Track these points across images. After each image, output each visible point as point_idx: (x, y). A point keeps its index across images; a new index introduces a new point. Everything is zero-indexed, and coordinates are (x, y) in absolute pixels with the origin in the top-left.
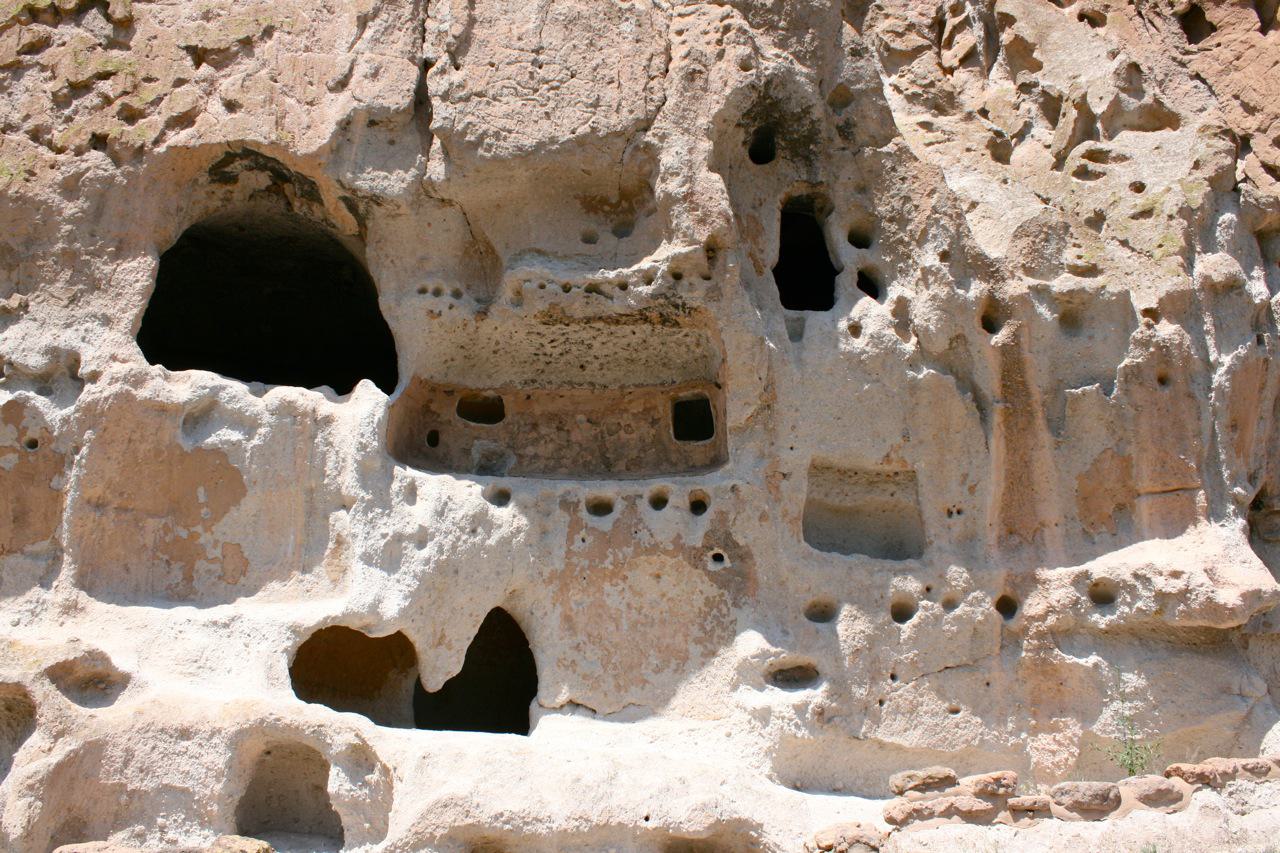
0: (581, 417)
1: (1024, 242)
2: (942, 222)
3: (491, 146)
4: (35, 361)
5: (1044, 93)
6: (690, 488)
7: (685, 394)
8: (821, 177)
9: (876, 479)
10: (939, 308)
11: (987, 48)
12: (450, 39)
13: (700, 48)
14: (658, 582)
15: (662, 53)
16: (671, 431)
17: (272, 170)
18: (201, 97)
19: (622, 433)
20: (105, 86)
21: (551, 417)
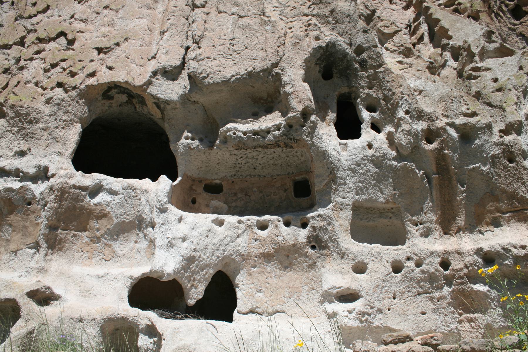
2: (405, 98)
4: (32, 171)
5: (452, 47)
7: (299, 178)
9: (383, 211)
14: (288, 258)
16: (293, 194)
17: (127, 93)
18: (100, 66)
19: (272, 195)
20: (63, 64)
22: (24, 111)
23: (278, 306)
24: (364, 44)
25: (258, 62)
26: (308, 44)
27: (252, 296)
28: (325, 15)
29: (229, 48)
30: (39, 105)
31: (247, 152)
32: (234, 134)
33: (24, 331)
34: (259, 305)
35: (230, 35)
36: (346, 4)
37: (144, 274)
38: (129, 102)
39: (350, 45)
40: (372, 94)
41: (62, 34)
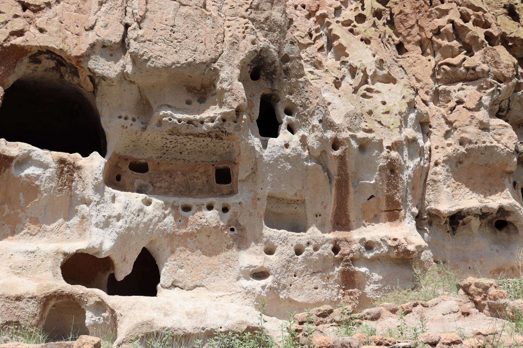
0: (179, 173)
1: (348, 119)
2: (320, 109)
3: (153, 62)
5: (350, 65)
6: (222, 202)
7: (221, 166)
8: (276, 88)
9: (290, 202)
10: (318, 140)
11: (328, 46)
12: (138, 17)
13: (236, 34)
15: (222, 34)
16: (215, 180)
17: (57, 60)
21: (167, 172)
23: (198, 281)
25: (198, 54)
28: (261, 21)
29: (170, 35)
31: (178, 138)
32: (170, 120)
34: (181, 280)
36: (279, 14)
38: (56, 68)
39: (279, 52)
40: (291, 99)
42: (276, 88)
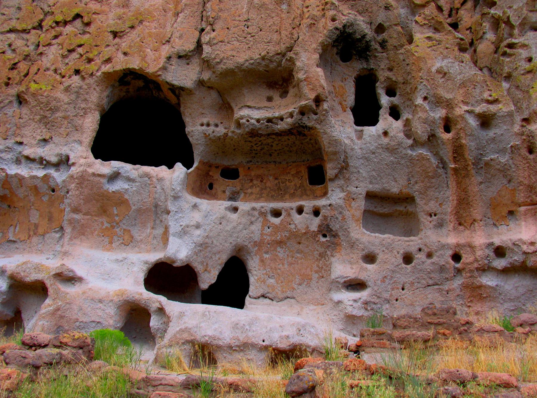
2: (424, 83)
4: (54, 159)
6: (312, 205)
19: (287, 182)
20: (80, 50)
22: (45, 100)
24: (385, 22)
26: (323, 26)
27: (264, 282)
30: (59, 94)
32: (248, 121)
33: (51, 308)
34: (270, 291)
35: (245, 16)
37: (158, 260)
40: (391, 77)
41: (78, 16)
42: (372, 67)
